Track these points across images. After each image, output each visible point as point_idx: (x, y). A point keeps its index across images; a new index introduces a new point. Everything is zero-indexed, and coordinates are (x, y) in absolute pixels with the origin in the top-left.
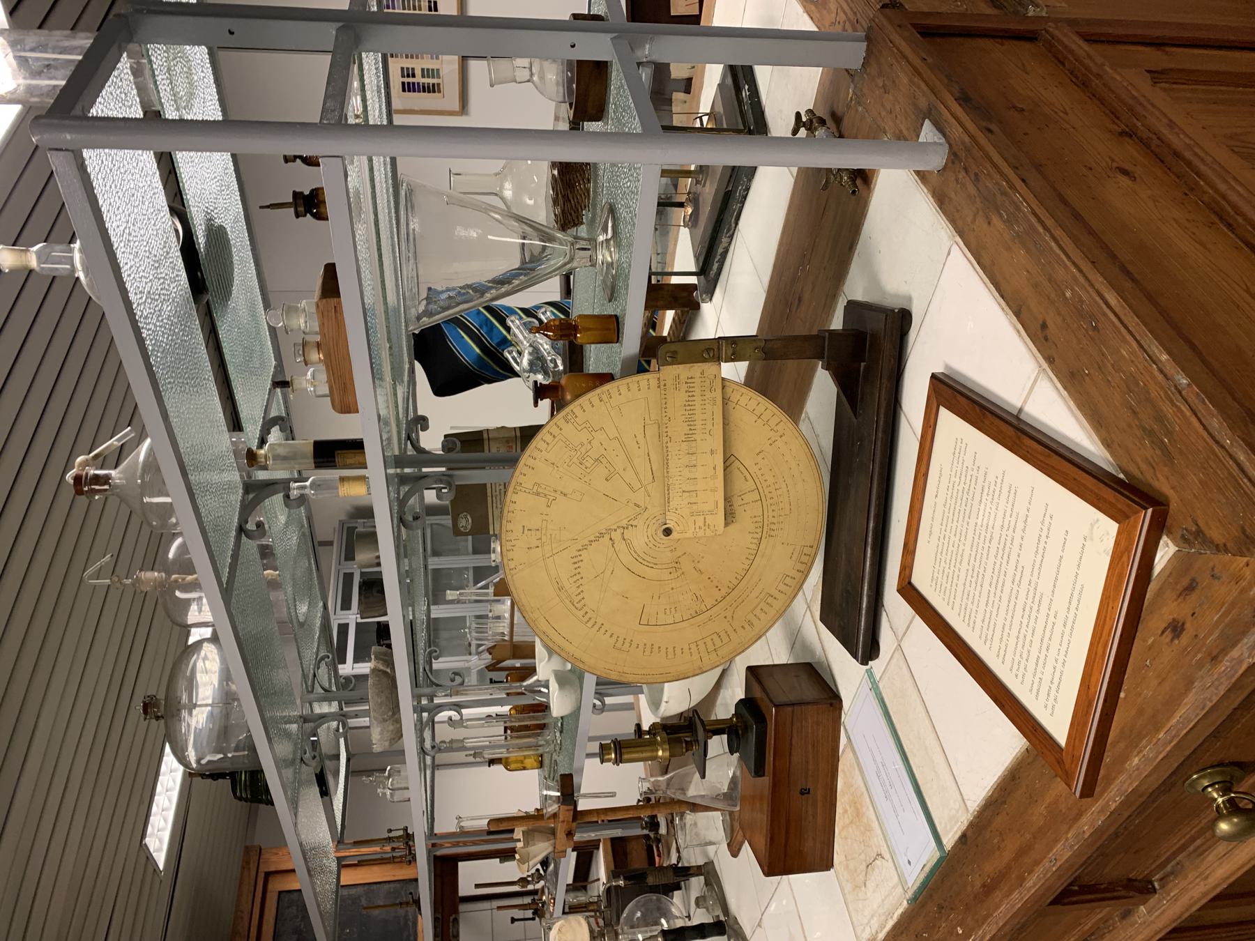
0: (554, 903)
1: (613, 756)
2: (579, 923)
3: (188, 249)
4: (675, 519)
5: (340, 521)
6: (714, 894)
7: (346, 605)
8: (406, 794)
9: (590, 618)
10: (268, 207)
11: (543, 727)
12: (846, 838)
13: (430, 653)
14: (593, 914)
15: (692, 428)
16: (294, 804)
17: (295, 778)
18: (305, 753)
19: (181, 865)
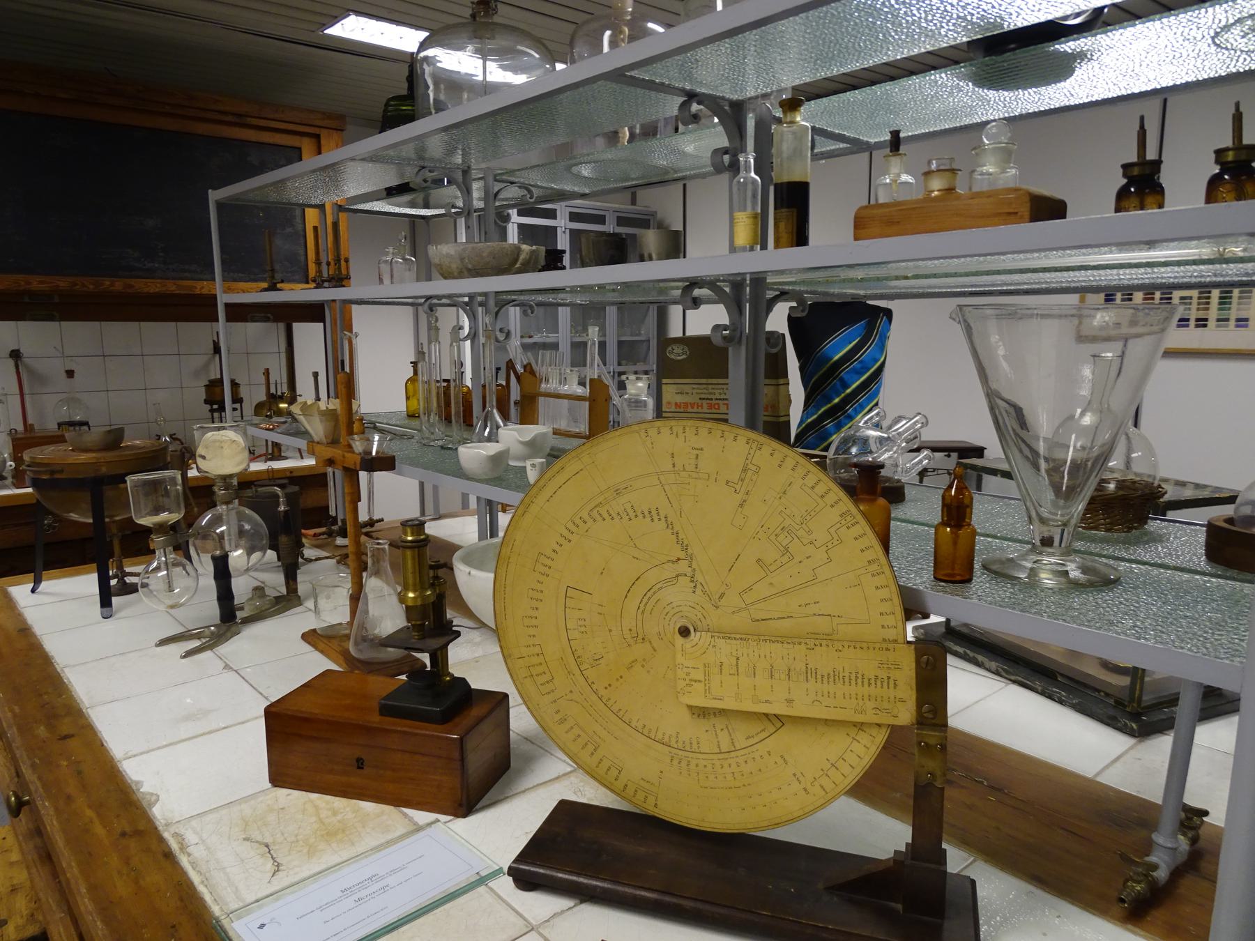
0: (268, 429)
1: (410, 538)
2: (238, 464)
3: (1052, 31)
4: (701, 643)
5: (656, 212)
6: (267, 607)
7: (574, 217)
8: (387, 281)
9: (578, 526)
10: (1142, 126)
11: (448, 420)
12: (304, 811)
13: (531, 307)
14: (270, 451)
15: (825, 679)
16: (374, 158)
17: (404, 160)
18: (430, 171)
19: (330, 52)
